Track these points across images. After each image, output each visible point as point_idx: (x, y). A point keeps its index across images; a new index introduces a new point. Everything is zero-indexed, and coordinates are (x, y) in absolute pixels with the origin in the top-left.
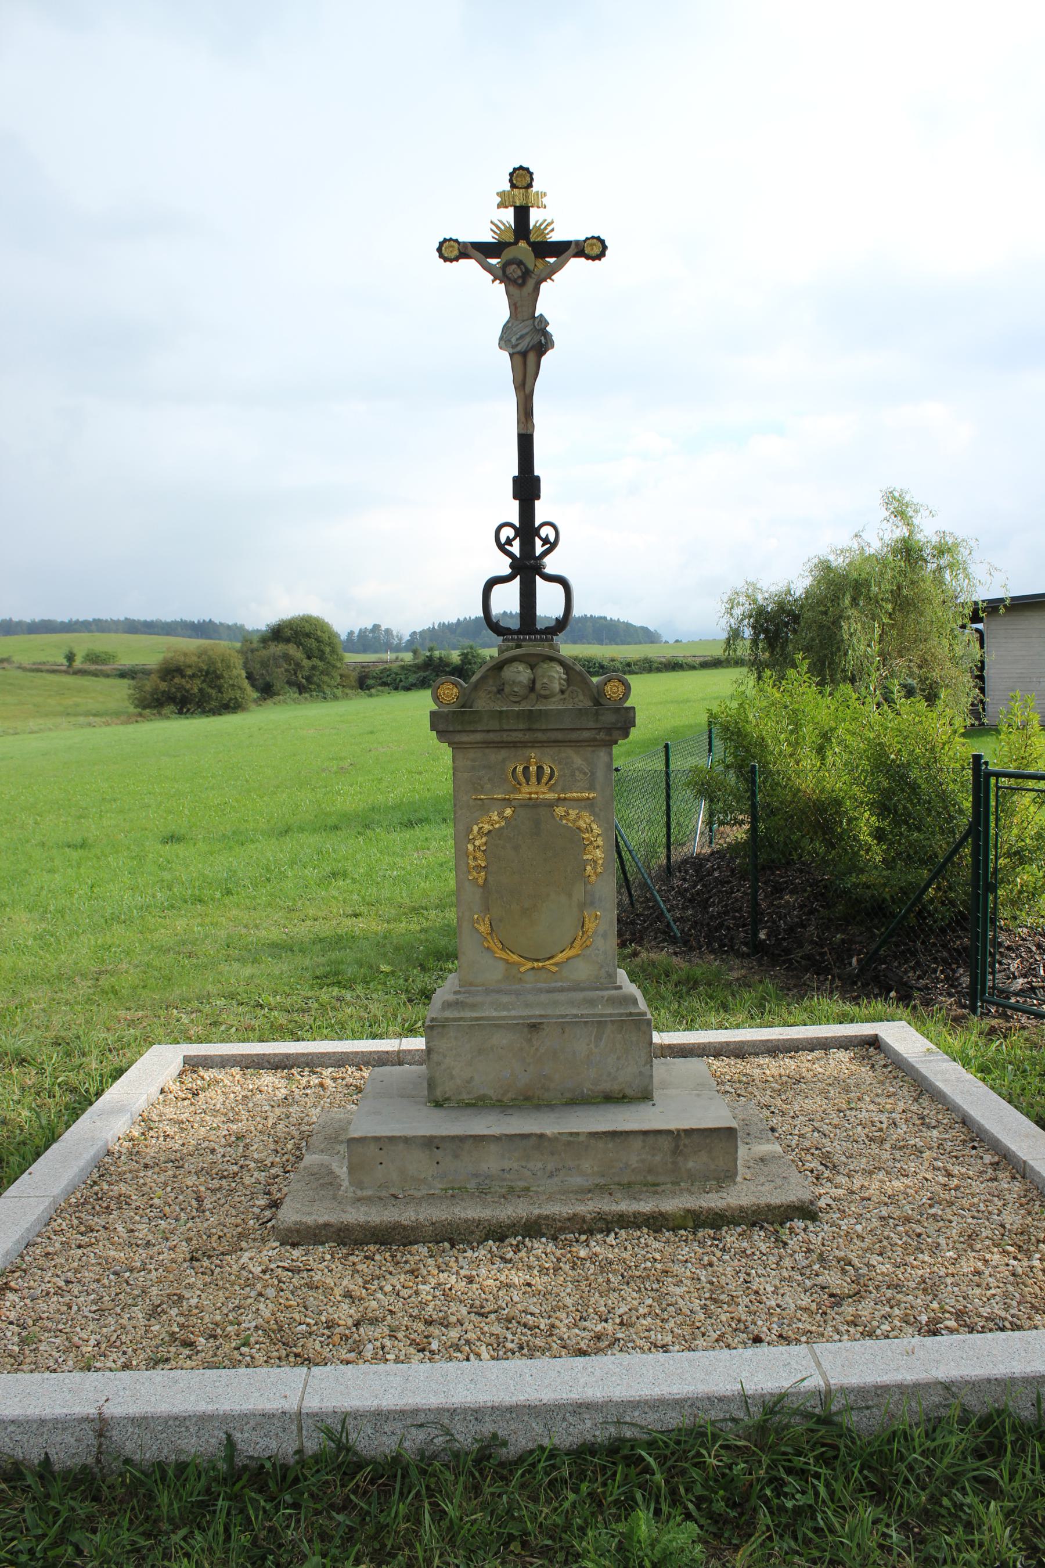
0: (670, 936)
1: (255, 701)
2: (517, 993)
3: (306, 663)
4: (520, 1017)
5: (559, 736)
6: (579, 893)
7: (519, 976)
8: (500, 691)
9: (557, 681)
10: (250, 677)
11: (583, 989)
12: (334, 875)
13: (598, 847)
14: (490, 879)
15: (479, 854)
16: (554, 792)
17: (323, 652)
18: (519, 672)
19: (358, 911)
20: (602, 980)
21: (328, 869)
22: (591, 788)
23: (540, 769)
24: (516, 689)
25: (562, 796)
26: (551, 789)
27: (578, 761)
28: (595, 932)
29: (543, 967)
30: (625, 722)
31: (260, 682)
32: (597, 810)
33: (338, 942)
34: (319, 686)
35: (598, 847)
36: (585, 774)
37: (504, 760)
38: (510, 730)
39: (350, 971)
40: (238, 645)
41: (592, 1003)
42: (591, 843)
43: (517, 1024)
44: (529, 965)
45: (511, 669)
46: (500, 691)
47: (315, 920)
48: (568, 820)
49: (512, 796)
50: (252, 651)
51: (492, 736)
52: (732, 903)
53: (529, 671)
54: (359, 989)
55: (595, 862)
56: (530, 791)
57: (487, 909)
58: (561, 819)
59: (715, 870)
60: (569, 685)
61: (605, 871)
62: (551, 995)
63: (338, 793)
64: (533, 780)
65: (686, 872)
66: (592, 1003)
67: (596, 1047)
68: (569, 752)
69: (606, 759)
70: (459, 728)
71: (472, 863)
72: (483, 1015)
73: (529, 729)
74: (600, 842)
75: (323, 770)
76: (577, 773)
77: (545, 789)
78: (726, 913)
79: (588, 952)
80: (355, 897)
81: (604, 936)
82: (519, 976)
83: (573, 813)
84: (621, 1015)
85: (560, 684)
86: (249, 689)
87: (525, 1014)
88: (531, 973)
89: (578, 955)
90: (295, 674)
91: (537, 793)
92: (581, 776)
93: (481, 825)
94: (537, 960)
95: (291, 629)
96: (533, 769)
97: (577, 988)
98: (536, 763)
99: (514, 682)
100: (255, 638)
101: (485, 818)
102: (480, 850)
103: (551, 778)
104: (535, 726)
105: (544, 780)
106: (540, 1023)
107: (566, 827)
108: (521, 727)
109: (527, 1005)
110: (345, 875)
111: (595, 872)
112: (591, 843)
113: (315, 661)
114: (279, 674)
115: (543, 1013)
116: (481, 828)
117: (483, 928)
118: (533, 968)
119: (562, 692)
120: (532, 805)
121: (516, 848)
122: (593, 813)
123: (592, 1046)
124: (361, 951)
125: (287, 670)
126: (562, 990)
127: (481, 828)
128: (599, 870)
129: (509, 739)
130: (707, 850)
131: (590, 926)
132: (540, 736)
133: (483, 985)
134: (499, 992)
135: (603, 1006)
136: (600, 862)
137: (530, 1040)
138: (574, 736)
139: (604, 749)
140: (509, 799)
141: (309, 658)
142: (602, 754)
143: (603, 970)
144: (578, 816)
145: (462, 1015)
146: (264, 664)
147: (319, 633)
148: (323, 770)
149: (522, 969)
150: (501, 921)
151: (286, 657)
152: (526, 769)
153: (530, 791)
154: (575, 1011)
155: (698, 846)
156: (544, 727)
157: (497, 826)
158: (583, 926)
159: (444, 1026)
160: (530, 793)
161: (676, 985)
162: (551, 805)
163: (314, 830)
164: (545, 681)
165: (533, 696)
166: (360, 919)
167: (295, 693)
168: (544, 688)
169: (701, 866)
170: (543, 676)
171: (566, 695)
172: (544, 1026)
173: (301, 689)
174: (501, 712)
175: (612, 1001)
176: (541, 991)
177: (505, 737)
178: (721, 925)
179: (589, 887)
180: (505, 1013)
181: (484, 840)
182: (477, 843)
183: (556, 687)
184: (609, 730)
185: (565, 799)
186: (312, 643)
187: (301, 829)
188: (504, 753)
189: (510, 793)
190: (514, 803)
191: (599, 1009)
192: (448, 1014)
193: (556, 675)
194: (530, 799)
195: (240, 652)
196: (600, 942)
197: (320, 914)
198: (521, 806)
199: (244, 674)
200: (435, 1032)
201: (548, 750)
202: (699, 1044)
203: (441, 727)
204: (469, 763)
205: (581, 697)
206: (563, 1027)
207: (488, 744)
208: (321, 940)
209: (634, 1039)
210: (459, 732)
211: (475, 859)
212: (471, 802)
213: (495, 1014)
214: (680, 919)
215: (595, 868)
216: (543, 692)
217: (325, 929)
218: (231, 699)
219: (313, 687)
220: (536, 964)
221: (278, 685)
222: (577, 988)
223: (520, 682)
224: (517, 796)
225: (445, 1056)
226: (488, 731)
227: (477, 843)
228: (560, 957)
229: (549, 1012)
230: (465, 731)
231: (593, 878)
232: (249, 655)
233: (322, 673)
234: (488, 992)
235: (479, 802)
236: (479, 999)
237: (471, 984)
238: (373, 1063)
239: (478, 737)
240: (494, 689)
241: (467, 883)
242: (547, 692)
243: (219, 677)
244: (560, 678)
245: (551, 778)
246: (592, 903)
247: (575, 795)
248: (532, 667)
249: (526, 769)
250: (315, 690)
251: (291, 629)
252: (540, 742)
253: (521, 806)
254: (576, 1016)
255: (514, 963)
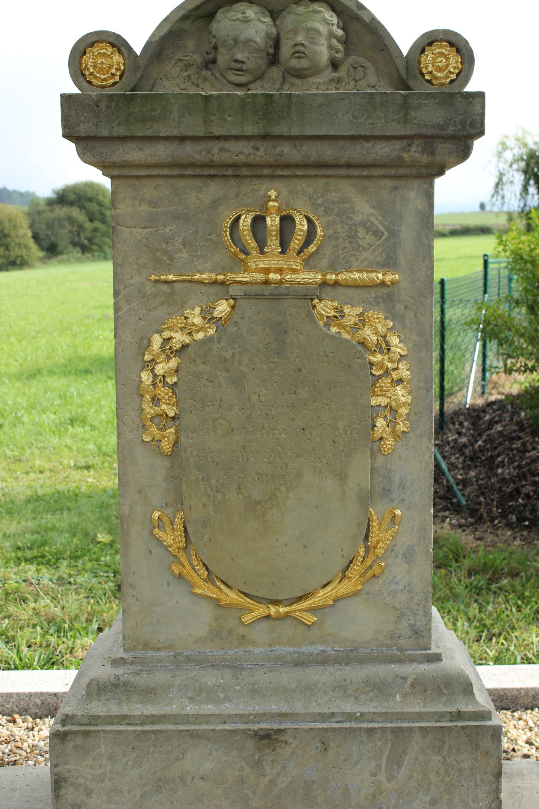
0: (452, 504)
1: (41, 260)
2: (237, 667)
3: (88, 225)
4: (242, 717)
5: (327, 152)
6: (359, 473)
7: (241, 630)
8: (210, 63)
9: (323, 41)
10: (36, 237)
11: (364, 661)
12: (72, 421)
13: (400, 381)
14: (184, 440)
15: (163, 392)
16: (314, 269)
17: (104, 215)
18: (246, 21)
19: (91, 463)
20: (402, 642)
21: (68, 416)
22: (390, 263)
23: (287, 221)
24: (240, 56)
25: (331, 277)
26: (309, 264)
27: (363, 208)
28: (391, 549)
29: (287, 615)
30: (463, 123)
31: (46, 243)
32: (400, 307)
33: (59, 502)
34: (100, 247)
35: (400, 381)
36: (377, 233)
37: (216, 203)
38: (227, 138)
39: (60, 541)
40: (26, 208)
41: (380, 689)
42: (387, 373)
43: (235, 731)
44: (260, 610)
45: (230, 15)
46: (210, 63)
47: (41, 472)
48: (341, 326)
49: (230, 276)
50: (39, 213)
51: (191, 151)
52: (528, 464)
53: (268, 19)
54: (64, 568)
55: (394, 411)
56: (267, 265)
57: (178, 500)
58: (327, 325)
59: (497, 422)
60: (347, 53)
61: (412, 429)
62: (300, 672)
63: (97, 338)
64: (273, 244)
65: (461, 424)
66: (380, 689)
67: (390, 779)
68: (347, 190)
69: (420, 204)
70: (122, 131)
71: (150, 410)
72: (167, 710)
73: (265, 137)
74: (404, 371)
75: (88, 317)
76: (361, 233)
77: (296, 263)
78: (523, 477)
79: (376, 586)
80: (91, 446)
81: (409, 556)
82: (241, 630)
83: (351, 313)
84: (440, 716)
85: (331, 47)
86: (34, 246)
87: (250, 710)
88: (264, 625)
89: (357, 593)
90: (78, 235)
91: (279, 271)
92: (370, 239)
93: (167, 334)
94: (276, 602)
95: (75, 193)
96: (273, 222)
97: (351, 656)
98: (279, 210)
99: (236, 41)
100: (42, 203)
101: (177, 321)
102: (165, 383)
103: (308, 242)
104: (277, 130)
105: (295, 244)
106: (279, 731)
107: (336, 339)
108: (249, 130)
109: (255, 692)
110: (84, 421)
111: (393, 432)
112: (387, 373)
113: (97, 224)
114: (63, 235)
115: (285, 708)
116: (167, 340)
117: (171, 538)
118: (268, 617)
119: (335, 65)
120: (270, 294)
121: (237, 382)
122: (391, 314)
123: (382, 777)
124: (80, 514)
125: (70, 232)
126: (323, 661)
127: (167, 340)
128: (401, 427)
129: (226, 157)
130: (480, 402)
131: (381, 536)
132: (288, 151)
133: (171, 647)
134: (202, 662)
135: (404, 696)
136: (404, 411)
137: (259, 764)
138: (356, 152)
139: (416, 184)
140: (223, 283)
141: (91, 220)
142: (412, 194)
143: (404, 623)
144: (362, 321)
145: (125, 710)
146: (50, 226)
147: (101, 198)
148: (88, 317)
149: (247, 618)
150: (205, 524)
151: (70, 219)
152: (259, 221)
153: (267, 265)
154: (349, 707)
155: (470, 396)
156: (295, 132)
157: (200, 336)
158: (367, 537)
159: (87, 734)
160: (267, 271)
161: (470, 575)
162: (308, 295)
163: (66, 374)
164: (300, 39)
165: (275, 73)
166: (92, 472)
167: (78, 252)
168: (298, 54)
169: (479, 418)
170: (295, 31)
171: (342, 73)
172: (287, 737)
173: (84, 249)
174: (207, 98)
175: (420, 686)
176: (281, 662)
177: (217, 152)
178: (517, 491)
179: (380, 460)
180: (210, 708)
181: (173, 363)
182: (160, 369)
183: (323, 53)
184: (429, 140)
185: (336, 283)
186: (93, 207)
187: (51, 373)
188: (215, 189)
189: (225, 270)
190: (234, 290)
191: (398, 704)
192: (98, 708)
193: (323, 29)
194: (266, 282)
195: (29, 214)
196: (399, 569)
197: (47, 466)
198: (247, 296)
199: (29, 234)
200: (70, 745)
201: (303, 184)
202: (527, 690)
203: (83, 129)
204: (144, 208)
205: (372, 78)
206: (324, 740)
207: (183, 169)
208: (38, 499)
209: (466, 765)
210: (123, 139)
211: (155, 400)
212: (149, 288)
213: (190, 709)
214: (464, 483)
215: (392, 423)
216: (295, 63)
217: (45, 485)
218: (17, 257)
219: (95, 247)
220: (273, 610)
221: (62, 245)
222: (351, 656)
223: (249, 41)
224: (240, 277)
225: (89, 793)
226: (182, 139)
227: (160, 369)
228: (322, 597)
229: (299, 707)
230: (133, 138)
231: (390, 442)
232: (36, 217)
233: (103, 235)
234: (179, 661)
235: (165, 288)
236: (160, 677)
237: (147, 646)
238: (34, 710)
239: (161, 152)
240: (197, 58)
241: (139, 451)
242: (304, 63)
243: (6, 236)
244: (331, 35)
245: (308, 242)
246: (386, 492)
247: (356, 275)
248: (274, 15)
249: (259, 221)
250: (96, 251)
251: (75, 193)
252: (288, 166)
253: (247, 296)
254: (350, 717)
255: (230, 607)
